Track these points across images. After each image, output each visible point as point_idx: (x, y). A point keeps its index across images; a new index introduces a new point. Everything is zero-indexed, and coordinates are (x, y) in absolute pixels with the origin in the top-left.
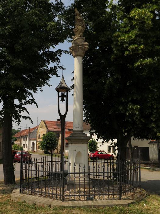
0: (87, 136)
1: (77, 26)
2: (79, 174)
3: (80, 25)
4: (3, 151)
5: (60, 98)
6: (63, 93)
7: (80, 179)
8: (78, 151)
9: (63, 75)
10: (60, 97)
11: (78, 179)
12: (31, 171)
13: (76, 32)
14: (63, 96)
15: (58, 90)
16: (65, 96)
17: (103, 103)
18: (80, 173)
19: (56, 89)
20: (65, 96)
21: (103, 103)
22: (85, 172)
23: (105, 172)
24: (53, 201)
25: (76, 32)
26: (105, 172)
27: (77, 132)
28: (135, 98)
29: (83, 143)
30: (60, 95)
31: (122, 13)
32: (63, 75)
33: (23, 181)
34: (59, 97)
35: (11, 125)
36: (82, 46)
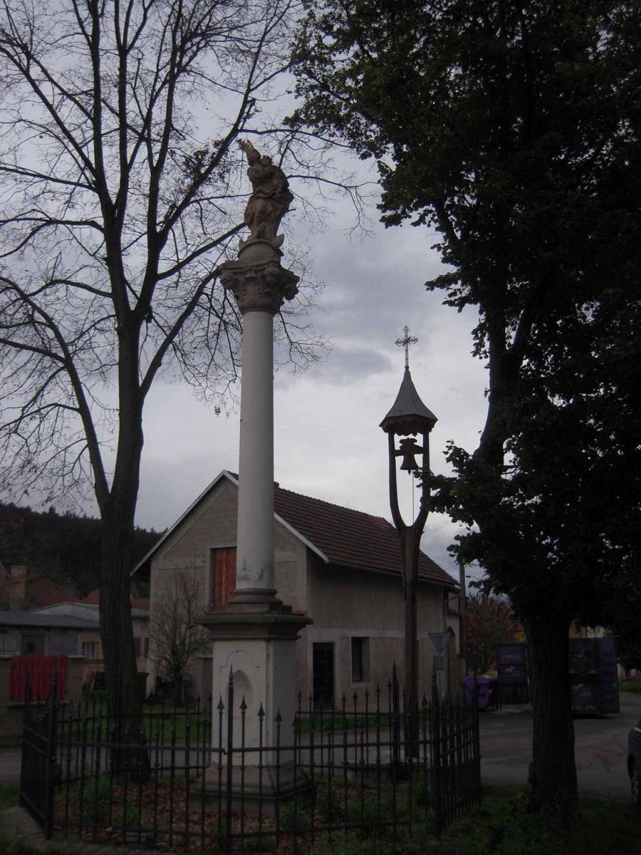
0: (430, 513)
5: (400, 460)
6: (411, 436)
9: (407, 367)
10: (399, 453)
12: (183, 753)
14: (409, 450)
16: (419, 450)
17: (579, 376)
19: (380, 426)
20: (419, 450)
21: (579, 376)
23: (355, 746)
26: (355, 746)
30: (398, 446)
31: (577, 16)
32: (407, 367)
33: (60, 725)
34: (393, 454)
35: (65, 354)
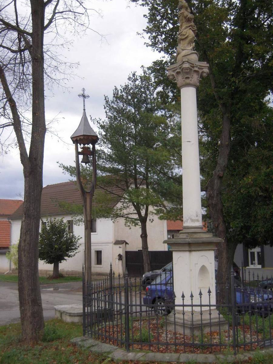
1: (185, 29)
2: (182, 307)
3: (190, 28)
4: (24, 259)
7: (202, 315)
8: (202, 265)
11: (181, 316)
13: (183, 40)
15: (76, 140)
18: (183, 306)
22: (137, 311)
24: (117, 349)
25: (183, 40)
27: (196, 230)
28: (147, 92)
29: (85, 251)
30: (80, 150)
32: (84, 110)
34: (78, 153)
36: (199, 68)
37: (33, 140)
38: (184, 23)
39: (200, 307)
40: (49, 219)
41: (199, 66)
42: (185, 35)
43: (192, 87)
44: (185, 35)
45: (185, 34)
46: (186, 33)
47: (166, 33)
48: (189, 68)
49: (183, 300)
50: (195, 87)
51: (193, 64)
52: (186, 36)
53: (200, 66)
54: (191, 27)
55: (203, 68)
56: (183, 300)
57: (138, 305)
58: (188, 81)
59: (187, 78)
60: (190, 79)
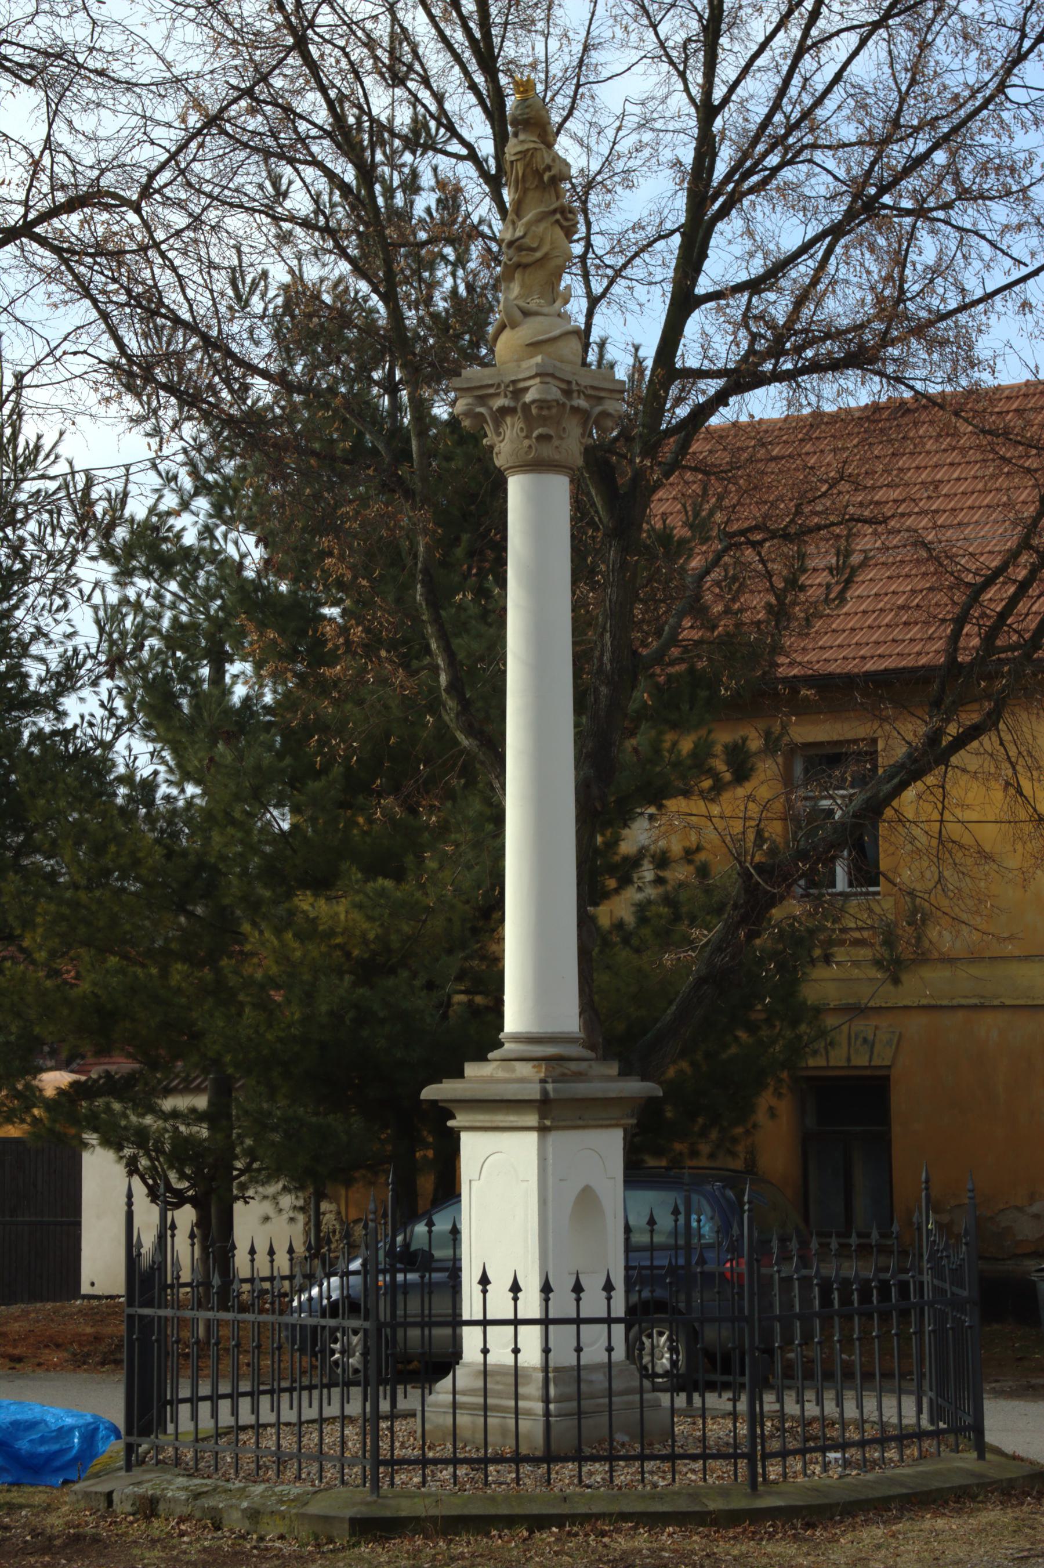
37: (602, 978)
38: (530, 194)
39: (574, 1327)
40: (870, 1404)
41: (590, 392)
42: (534, 250)
43: (558, 472)
44: (534, 250)
45: (535, 245)
46: (542, 240)
47: (405, 148)
48: (557, 401)
49: (578, 1300)
50: (566, 474)
51: (569, 383)
52: (538, 255)
53: (593, 388)
54: (558, 216)
55: (602, 394)
56: (578, 1300)
57: (743, 1456)
58: (547, 451)
59: (543, 438)
60: (556, 442)
